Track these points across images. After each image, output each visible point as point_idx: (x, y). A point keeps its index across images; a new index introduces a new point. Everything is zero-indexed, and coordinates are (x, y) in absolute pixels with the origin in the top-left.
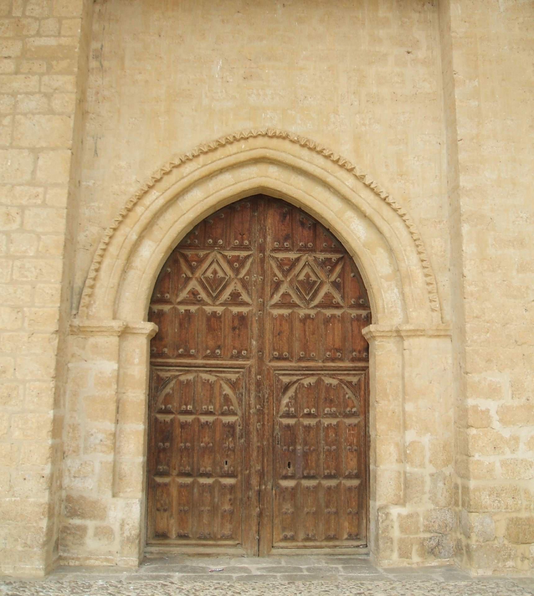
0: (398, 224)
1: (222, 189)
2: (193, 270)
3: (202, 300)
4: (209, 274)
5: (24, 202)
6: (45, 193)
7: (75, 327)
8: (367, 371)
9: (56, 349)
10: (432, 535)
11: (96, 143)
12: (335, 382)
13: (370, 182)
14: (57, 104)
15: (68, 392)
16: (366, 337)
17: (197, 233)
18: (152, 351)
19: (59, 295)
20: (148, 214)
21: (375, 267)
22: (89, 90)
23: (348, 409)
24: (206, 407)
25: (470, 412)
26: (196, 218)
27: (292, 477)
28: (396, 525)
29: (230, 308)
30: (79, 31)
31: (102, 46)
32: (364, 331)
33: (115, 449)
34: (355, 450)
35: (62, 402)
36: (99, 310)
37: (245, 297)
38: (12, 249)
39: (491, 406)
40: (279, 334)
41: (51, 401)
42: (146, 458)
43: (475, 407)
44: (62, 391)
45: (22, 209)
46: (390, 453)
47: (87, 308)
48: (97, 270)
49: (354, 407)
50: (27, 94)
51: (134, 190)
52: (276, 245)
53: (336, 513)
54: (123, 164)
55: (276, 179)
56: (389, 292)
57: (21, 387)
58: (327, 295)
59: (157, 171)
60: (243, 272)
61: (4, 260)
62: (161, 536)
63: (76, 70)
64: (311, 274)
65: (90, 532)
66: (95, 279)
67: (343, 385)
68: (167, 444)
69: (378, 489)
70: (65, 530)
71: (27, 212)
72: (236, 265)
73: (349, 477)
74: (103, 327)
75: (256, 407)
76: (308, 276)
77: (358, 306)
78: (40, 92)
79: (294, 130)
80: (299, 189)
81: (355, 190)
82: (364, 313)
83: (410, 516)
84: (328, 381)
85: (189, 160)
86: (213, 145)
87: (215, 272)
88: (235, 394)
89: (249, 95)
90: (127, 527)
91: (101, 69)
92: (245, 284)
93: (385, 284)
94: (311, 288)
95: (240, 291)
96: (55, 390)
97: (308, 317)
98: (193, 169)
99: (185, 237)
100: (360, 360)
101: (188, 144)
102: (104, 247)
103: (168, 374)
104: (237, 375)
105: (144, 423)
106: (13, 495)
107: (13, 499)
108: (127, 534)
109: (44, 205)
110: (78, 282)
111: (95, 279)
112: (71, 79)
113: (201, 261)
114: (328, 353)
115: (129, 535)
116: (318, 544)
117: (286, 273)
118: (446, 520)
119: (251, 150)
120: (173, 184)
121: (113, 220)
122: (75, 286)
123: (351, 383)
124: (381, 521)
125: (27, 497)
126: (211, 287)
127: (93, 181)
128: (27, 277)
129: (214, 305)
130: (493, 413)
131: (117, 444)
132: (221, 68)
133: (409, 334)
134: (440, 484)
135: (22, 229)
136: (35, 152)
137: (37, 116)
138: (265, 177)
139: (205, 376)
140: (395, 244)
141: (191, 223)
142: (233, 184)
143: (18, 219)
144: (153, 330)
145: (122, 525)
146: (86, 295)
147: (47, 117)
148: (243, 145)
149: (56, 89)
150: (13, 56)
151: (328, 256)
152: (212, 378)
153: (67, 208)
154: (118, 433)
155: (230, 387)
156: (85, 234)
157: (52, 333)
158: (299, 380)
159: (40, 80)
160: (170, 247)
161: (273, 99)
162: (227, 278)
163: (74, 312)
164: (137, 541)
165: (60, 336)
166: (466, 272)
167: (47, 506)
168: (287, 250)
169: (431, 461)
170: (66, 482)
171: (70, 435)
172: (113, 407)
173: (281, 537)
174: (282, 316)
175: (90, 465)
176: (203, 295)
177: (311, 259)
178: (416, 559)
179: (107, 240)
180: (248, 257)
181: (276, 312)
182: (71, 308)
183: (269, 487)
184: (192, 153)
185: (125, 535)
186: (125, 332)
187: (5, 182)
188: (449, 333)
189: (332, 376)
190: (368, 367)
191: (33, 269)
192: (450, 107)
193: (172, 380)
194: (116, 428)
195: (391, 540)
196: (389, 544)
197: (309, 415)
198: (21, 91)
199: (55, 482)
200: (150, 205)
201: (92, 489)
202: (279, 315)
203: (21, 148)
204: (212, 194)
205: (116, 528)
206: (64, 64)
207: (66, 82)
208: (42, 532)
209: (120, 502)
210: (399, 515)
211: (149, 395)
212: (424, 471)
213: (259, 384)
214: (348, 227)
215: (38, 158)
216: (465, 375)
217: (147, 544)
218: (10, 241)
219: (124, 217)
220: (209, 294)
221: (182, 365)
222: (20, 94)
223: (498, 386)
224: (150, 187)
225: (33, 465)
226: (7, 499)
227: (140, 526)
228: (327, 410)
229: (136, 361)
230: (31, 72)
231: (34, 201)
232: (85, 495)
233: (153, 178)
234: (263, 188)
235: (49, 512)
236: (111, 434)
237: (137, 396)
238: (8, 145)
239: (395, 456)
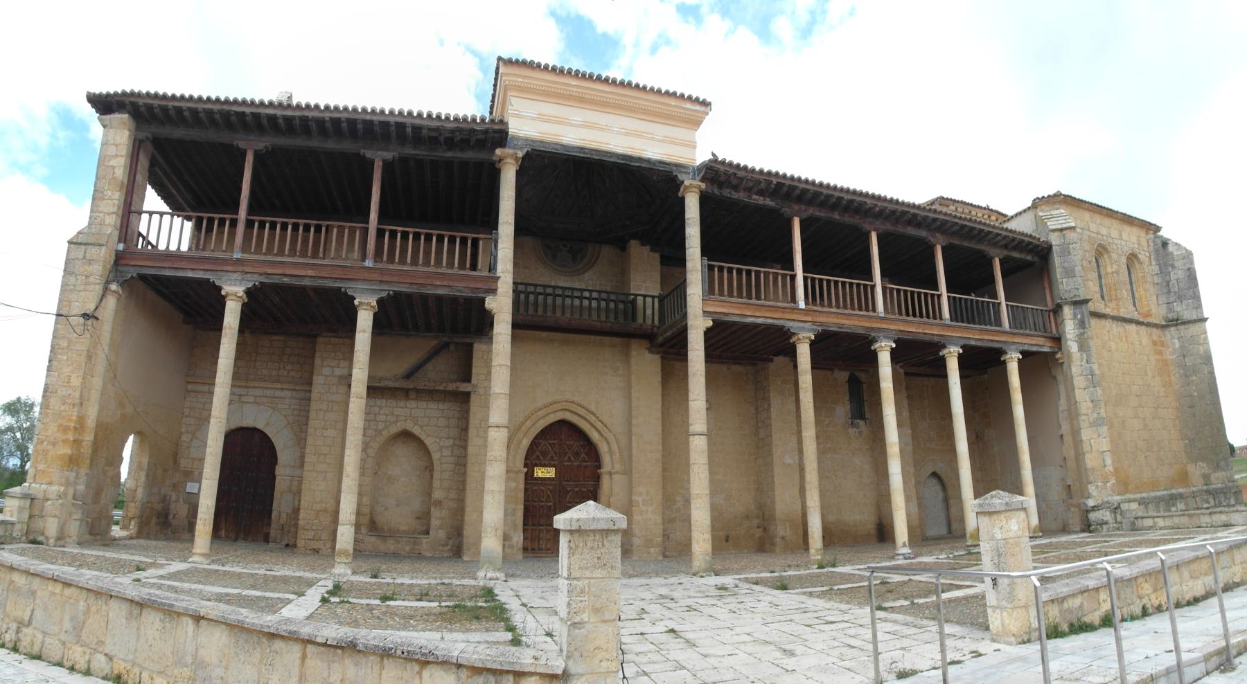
21: (603, 448)
79: (576, 399)
101: (539, 405)
116: (1027, 332)
192: (630, 393)
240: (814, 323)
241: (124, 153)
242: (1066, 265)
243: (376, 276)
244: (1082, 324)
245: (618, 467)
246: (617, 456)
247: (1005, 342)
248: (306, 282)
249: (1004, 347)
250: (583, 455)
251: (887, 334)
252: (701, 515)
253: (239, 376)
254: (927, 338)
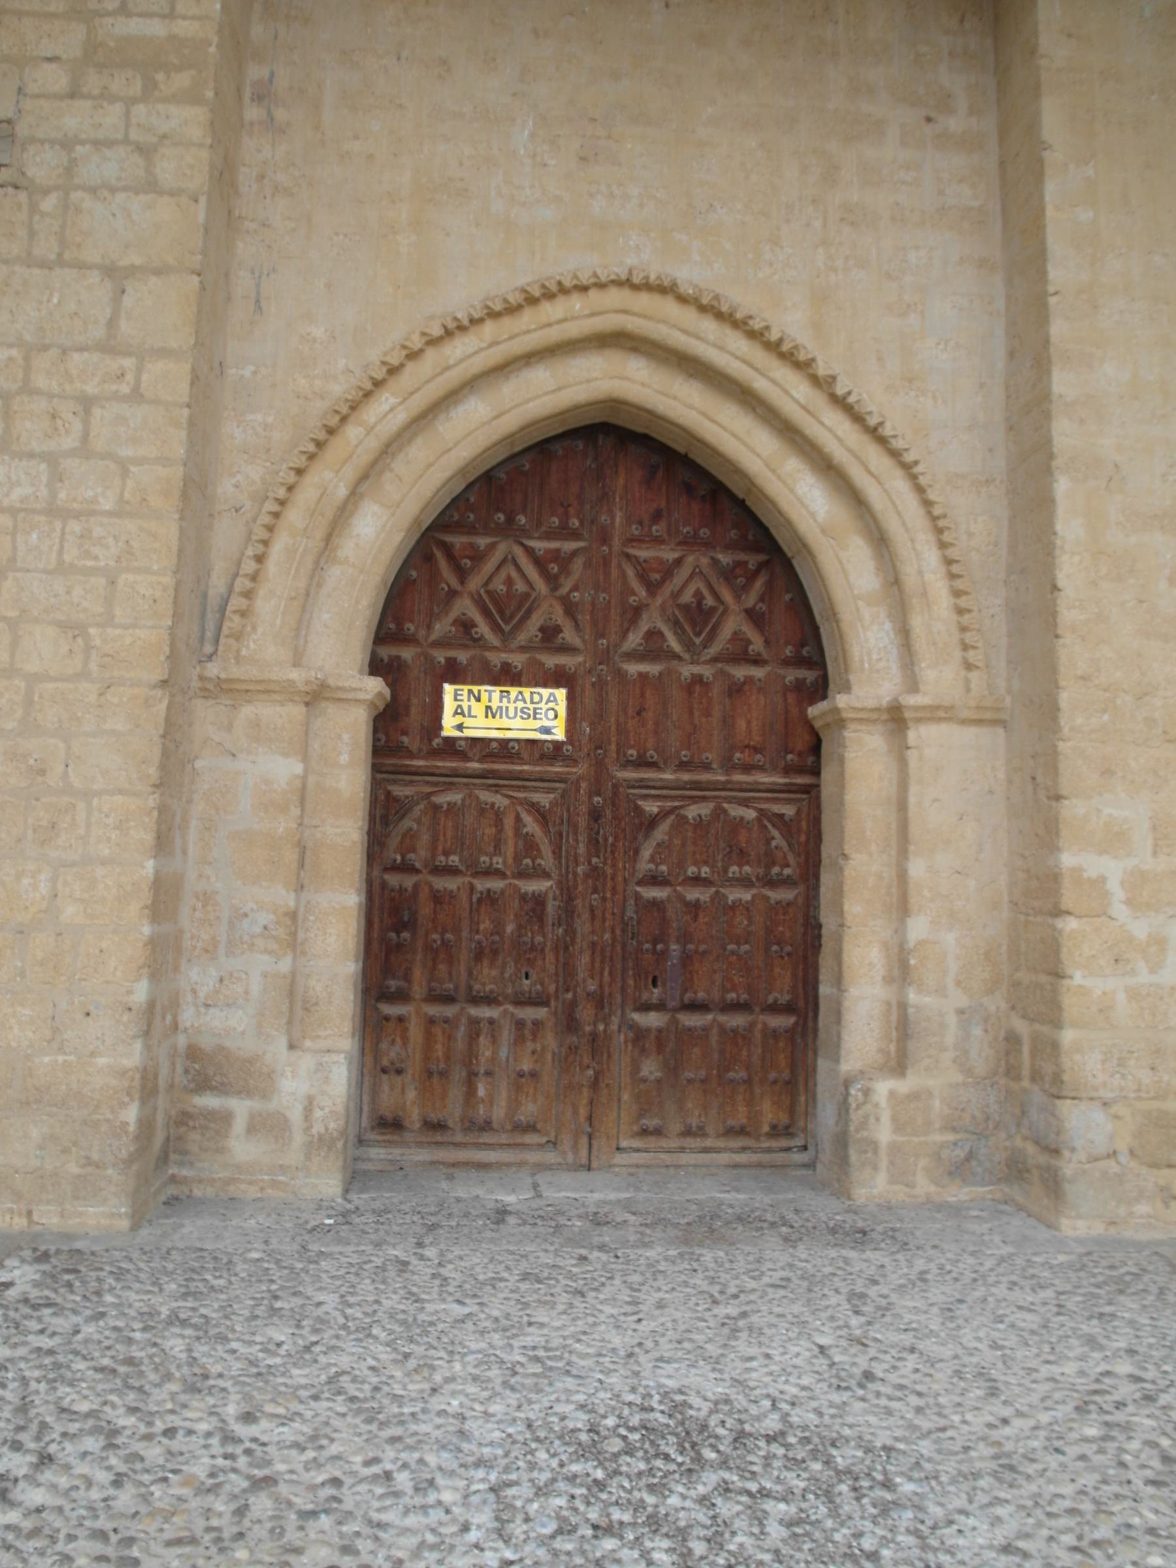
0: (899, 484)
1: (528, 401)
2: (462, 575)
3: (482, 638)
4: (499, 586)
5: (91, 389)
6: (139, 370)
7: (210, 679)
8: (813, 794)
9: (162, 722)
10: (959, 1136)
11: (258, 285)
12: (751, 814)
13: (846, 390)
14: (166, 169)
15: (194, 823)
16: (817, 724)
17: (472, 500)
18: (376, 740)
19: (171, 600)
20: (373, 444)
21: (846, 574)
22: (243, 169)
23: (776, 870)
24: (487, 859)
25: (1067, 883)
26: (474, 460)
27: (660, 1007)
28: (886, 1117)
29: (538, 656)
30: (218, 6)
31: (272, 74)
32: (813, 711)
33: (294, 944)
34: (789, 954)
35: (178, 842)
36: (263, 647)
37: (569, 635)
38: (62, 495)
39: (1111, 869)
40: (639, 713)
41: (149, 837)
42: (361, 965)
43: (1077, 871)
44: (178, 820)
45: (86, 403)
46: (870, 964)
47: (237, 639)
48: (260, 559)
49: (788, 866)
50: (97, 143)
51: (340, 390)
52: (635, 530)
53: (748, 1082)
54: (318, 332)
55: (643, 384)
56: (875, 628)
57: (81, 805)
58: (737, 636)
59: (393, 349)
60: (567, 585)
61: (43, 518)
62: (390, 1125)
63: (210, 94)
64: (706, 593)
65: (239, 1124)
66: (254, 578)
67: (766, 822)
68: (406, 935)
69: (845, 1036)
70: (184, 1119)
71: (97, 412)
72: (554, 568)
73: (774, 1009)
74: (270, 681)
75: (590, 863)
76: (698, 594)
77: (799, 661)
78: (126, 141)
79: (687, 275)
80: (691, 407)
81: (811, 408)
82: (810, 676)
83: (914, 1096)
84: (736, 811)
85: (461, 328)
86: (515, 298)
87: (509, 582)
88: (547, 832)
89: (591, 195)
90: (318, 1114)
91: (270, 123)
92: (570, 610)
93: (866, 613)
94: (706, 623)
95: (559, 622)
96: (160, 813)
97: (698, 680)
98: (471, 350)
99: (448, 507)
100: (800, 770)
101: (460, 295)
102: (275, 508)
103: (408, 791)
104: (552, 796)
105: (358, 891)
106: (61, 1050)
107: (61, 1058)
108: (318, 1128)
109: (136, 396)
110: (217, 584)
111: (254, 578)
112: (198, 114)
113: (478, 557)
114: (738, 755)
115: (323, 1131)
116: (709, 1143)
117: (652, 588)
118: (987, 1106)
119: (593, 315)
120: (428, 381)
121: (296, 451)
122: (211, 592)
123: (782, 816)
124: (854, 1105)
125: (93, 1054)
126: (501, 612)
127: (252, 368)
128: (96, 558)
129: (505, 648)
130: (1114, 886)
131: (301, 935)
132: (532, 135)
133: (919, 715)
134: (977, 1031)
135: (84, 449)
136: (117, 276)
137: (121, 197)
138: (621, 378)
139: (485, 796)
140: (893, 526)
141: (462, 471)
142: (553, 391)
143: (77, 426)
144: (380, 694)
145: (308, 1110)
146: (235, 612)
147: (142, 197)
148: (577, 303)
149: (164, 137)
150: (64, 57)
151: (742, 557)
152: (500, 801)
153: (188, 406)
154: (302, 911)
155: (537, 821)
156: (233, 481)
157: (154, 687)
158: (676, 808)
159: (127, 114)
160: (417, 521)
161: (641, 205)
162: (534, 595)
163: (208, 649)
164: (340, 1145)
165: (172, 696)
166: (1061, 581)
167: (138, 1076)
168: (658, 541)
169: (958, 983)
170: (187, 1016)
171: (198, 914)
172: (290, 856)
173: (635, 1128)
174: (643, 676)
175: (239, 979)
176: (483, 628)
177: (704, 561)
178: (924, 1186)
179: (282, 493)
180: (575, 553)
181: (633, 668)
182: (202, 639)
183: (614, 1027)
184: (470, 314)
185: (314, 1131)
187: (47, 341)
188: (1003, 716)
189: (745, 803)
190: (818, 786)
191: (111, 541)
193: (418, 804)
194: (298, 900)
195: (874, 1145)
196: (869, 1155)
197: (697, 880)
198: (83, 136)
199: (156, 1018)
200: (376, 424)
201: (243, 1033)
202: (640, 675)
203: (82, 266)
204: (509, 411)
205: (296, 1115)
206: (183, 80)
207: (188, 121)
208: (126, 1133)
209: (306, 1062)
210: (892, 1094)
211: (369, 833)
212: (940, 1002)
213: (595, 815)
214: (792, 491)
215: (123, 292)
216: (1054, 804)
217: (361, 1142)
218: (57, 477)
219: (320, 444)
220: (496, 628)
221: (438, 771)
222: (82, 143)
223: (1126, 826)
224: (378, 384)
225: (107, 982)
226: (47, 1059)
227: (347, 1110)
228: (734, 869)
229: (344, 758)
230: (106, 96)
231: (114, 387)
232: (228, 1043)
233: (384, 363)
234: (615, 404)
235: (143, 1087)
236: (286, 914)
237: (345, 832)
238: (53, 257)
239: (879, 971)
245: (940, 679)
246: (935, 618)
250: (733, 624)
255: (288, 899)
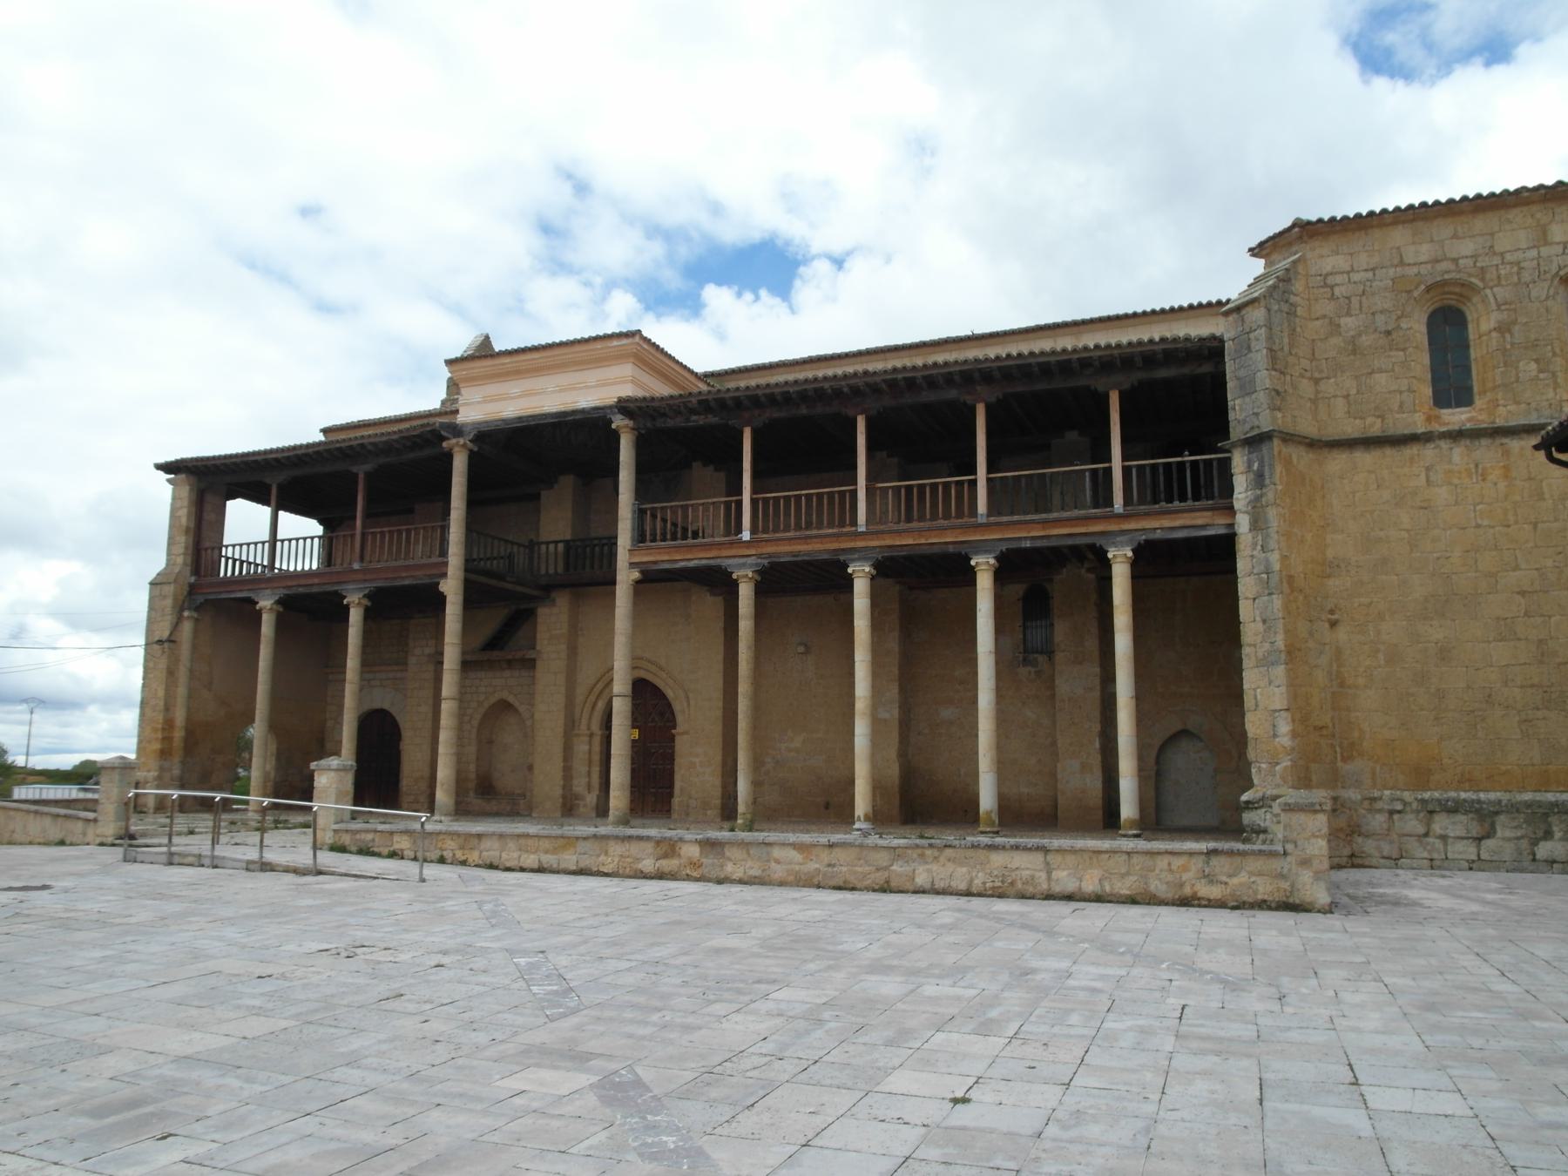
36: (583, 727)
39: (697, 760)
186: (591, 735)
240: (759, 556)
241: (186, 503)
242: (1242, 373)
243: (360, 576)
244: (1259, 480)
247: (1103, 533)
248: (315, 590)
249: (1099, 541)
251: (862, 553)
252: (444, 772)
253: (366, 664)
254: (936, 549)
255: (1276, 442)
